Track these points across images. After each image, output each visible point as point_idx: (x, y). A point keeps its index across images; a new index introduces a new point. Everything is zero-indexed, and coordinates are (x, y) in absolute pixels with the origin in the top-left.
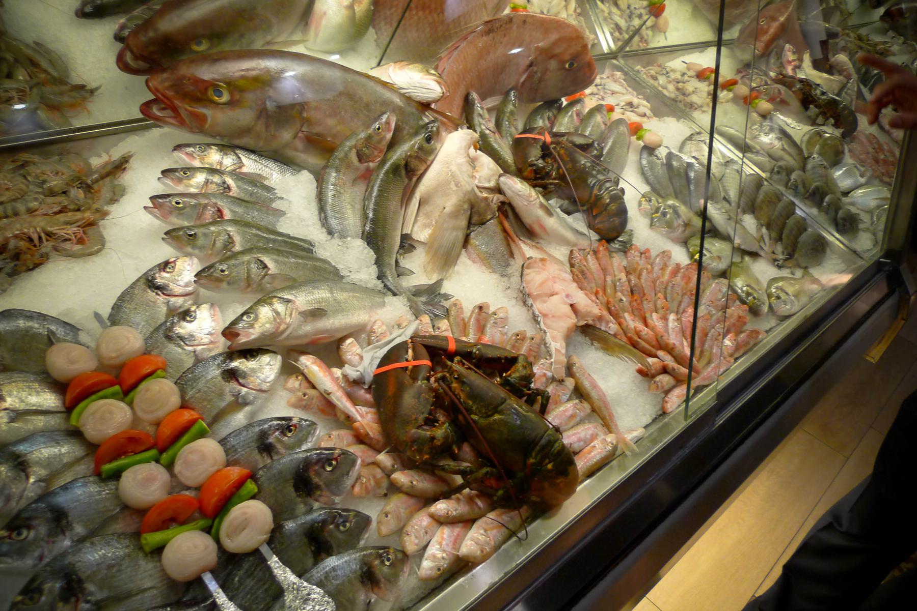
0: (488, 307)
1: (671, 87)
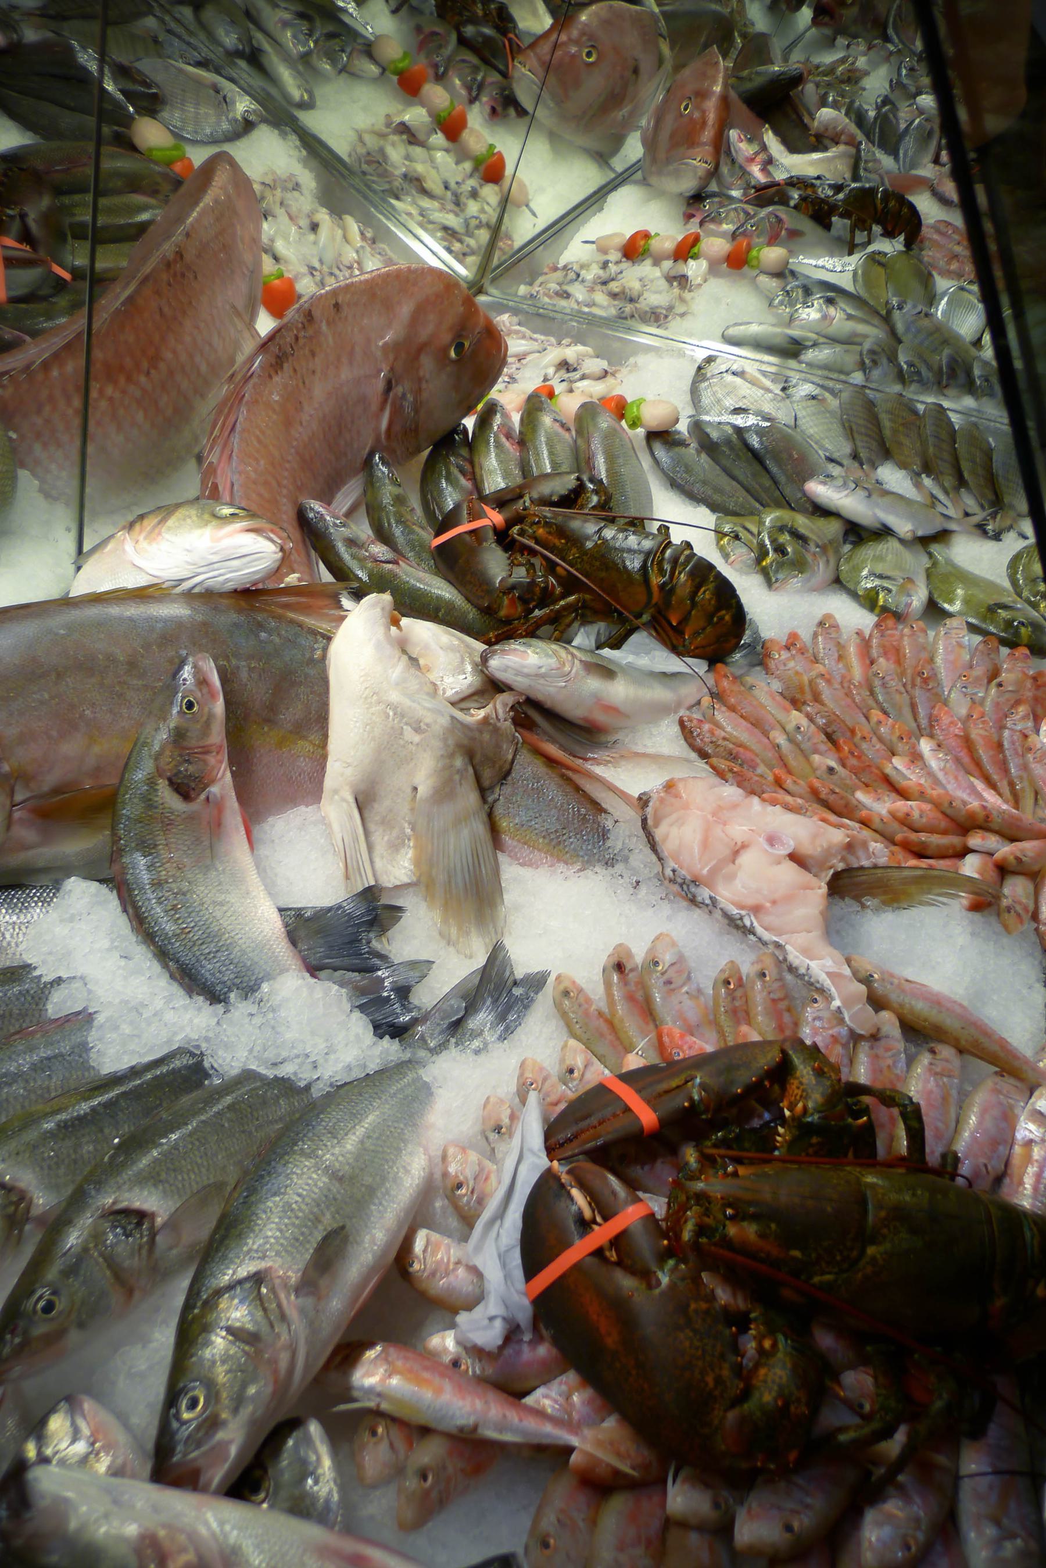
0: (630, 954)
1: (600, 297)
